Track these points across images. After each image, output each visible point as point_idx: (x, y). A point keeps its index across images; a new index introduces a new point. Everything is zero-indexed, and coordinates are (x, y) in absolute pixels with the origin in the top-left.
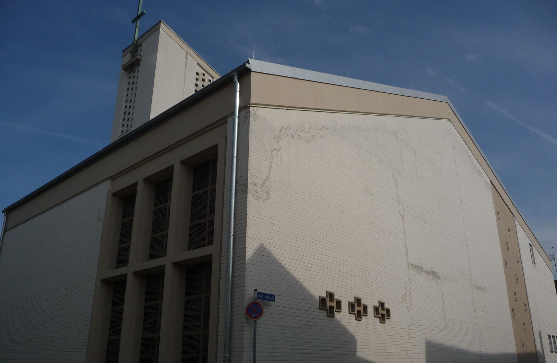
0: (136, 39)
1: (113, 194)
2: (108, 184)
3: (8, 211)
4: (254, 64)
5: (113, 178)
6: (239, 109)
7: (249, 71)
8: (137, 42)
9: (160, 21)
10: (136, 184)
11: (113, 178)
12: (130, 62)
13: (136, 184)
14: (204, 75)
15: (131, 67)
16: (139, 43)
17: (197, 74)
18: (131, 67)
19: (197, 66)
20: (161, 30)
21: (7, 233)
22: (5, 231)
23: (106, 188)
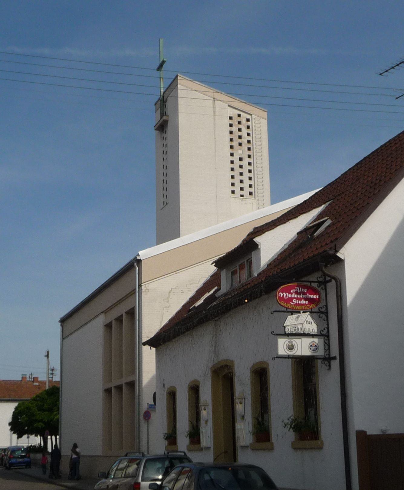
0: (162, 93)
1: (105, 326)
2: (102, 316)
3: (63, 321)
4: (143, 254)
5: (105, 312)
6: (135, 292)
7: (139, 262)
8: (163, 97)
9: (177, 76)
10: (122, 315)
11: (105, 312)
12: (159, 123)
13: (122, 315)
14: (239, 116)
15: (162, 127)
16: (165, 98)
17: (231, 118)
18: (162, 127)
19: (229, 108)
20: (179, 86)
21: (64, 341)
22: (63, 339)
23: (100, 322)
